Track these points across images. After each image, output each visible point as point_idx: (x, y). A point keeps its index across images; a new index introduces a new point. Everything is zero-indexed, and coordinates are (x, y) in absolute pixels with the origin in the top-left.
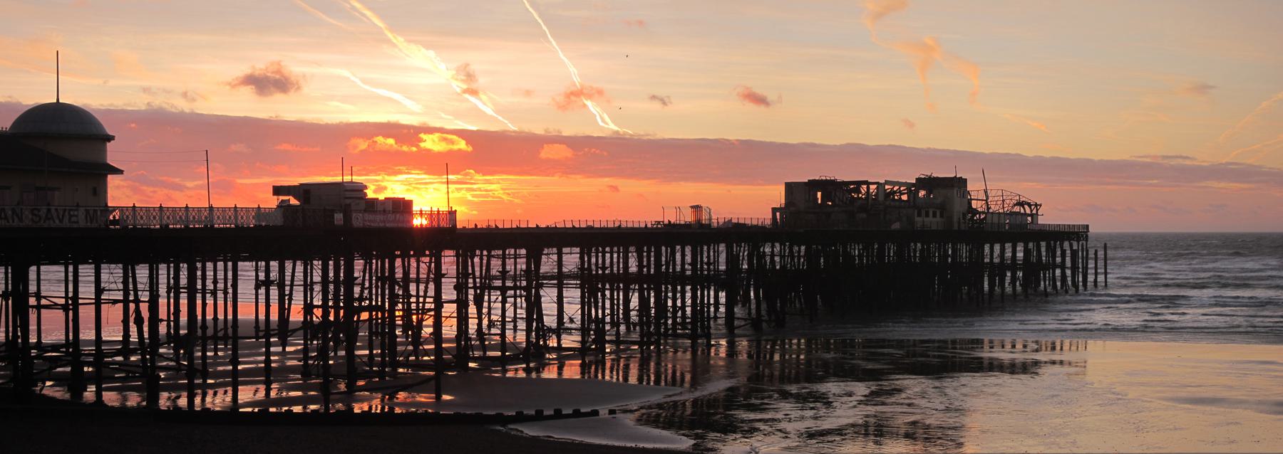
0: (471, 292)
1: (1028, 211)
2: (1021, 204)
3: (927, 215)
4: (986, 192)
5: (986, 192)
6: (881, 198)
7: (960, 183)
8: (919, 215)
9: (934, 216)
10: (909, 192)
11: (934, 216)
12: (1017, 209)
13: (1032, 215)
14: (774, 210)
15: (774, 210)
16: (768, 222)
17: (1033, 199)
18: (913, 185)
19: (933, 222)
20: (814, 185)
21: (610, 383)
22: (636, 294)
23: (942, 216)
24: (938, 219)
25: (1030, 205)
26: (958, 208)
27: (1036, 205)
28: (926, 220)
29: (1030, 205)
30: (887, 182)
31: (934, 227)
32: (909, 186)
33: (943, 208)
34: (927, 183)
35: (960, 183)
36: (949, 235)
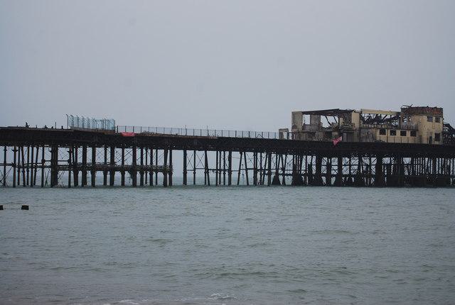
11: (403, 134)
18: (398, 113)
21: (330, 157)
23: (413, 134)
35: (436, 113)
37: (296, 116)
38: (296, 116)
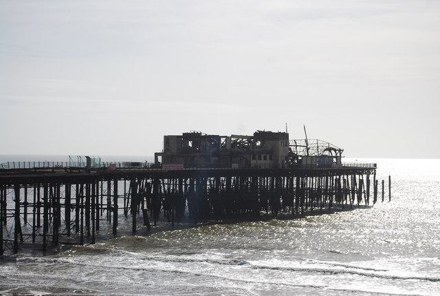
0: (84, 195)
1: (334, 154)
2: (329, 149)
3: (260, 159)
4: (306, 141)
5: (306, 141)
6: (229, 147)
7: (284, 137)
8: (254, 158)
9: (265, 159)
10: (249, 141)
11: (265, 159)
12: (327, 153)
13: (336, 157)
14: (157, 155)
15: (157, 155)
16: (153, 161)
17: (337, 146)
18: (252, 138)
19: (264, 163)
20: (187, 136)
21: (344, 175)
22: (71, 219)
23: (270, 158)
24: (268, 161)
25: (335, 150)
26: (282, 153)
27: (340, 150)
28: (259, 162)
29: (335, 150)
30: (233, 136)
31: (267, 167)
32: (249, 138)
33: (272, 153)
34: (260, 135)
35: (284, 137)
36: (277, 172)
37: (168, 140)
38: (168, 140)
